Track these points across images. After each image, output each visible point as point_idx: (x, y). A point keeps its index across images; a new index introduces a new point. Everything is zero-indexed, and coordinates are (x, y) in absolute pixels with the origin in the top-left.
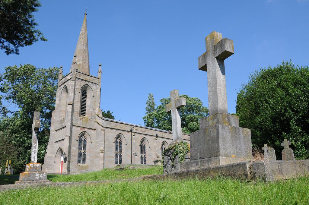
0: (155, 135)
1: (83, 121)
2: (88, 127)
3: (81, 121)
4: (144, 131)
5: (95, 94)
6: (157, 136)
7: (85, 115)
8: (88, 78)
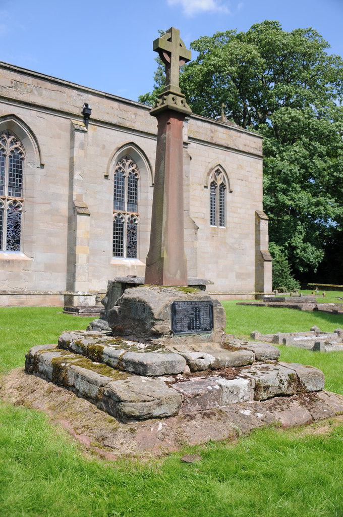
0: (78, 111)
4: (16, 85)
6: (86, 115)
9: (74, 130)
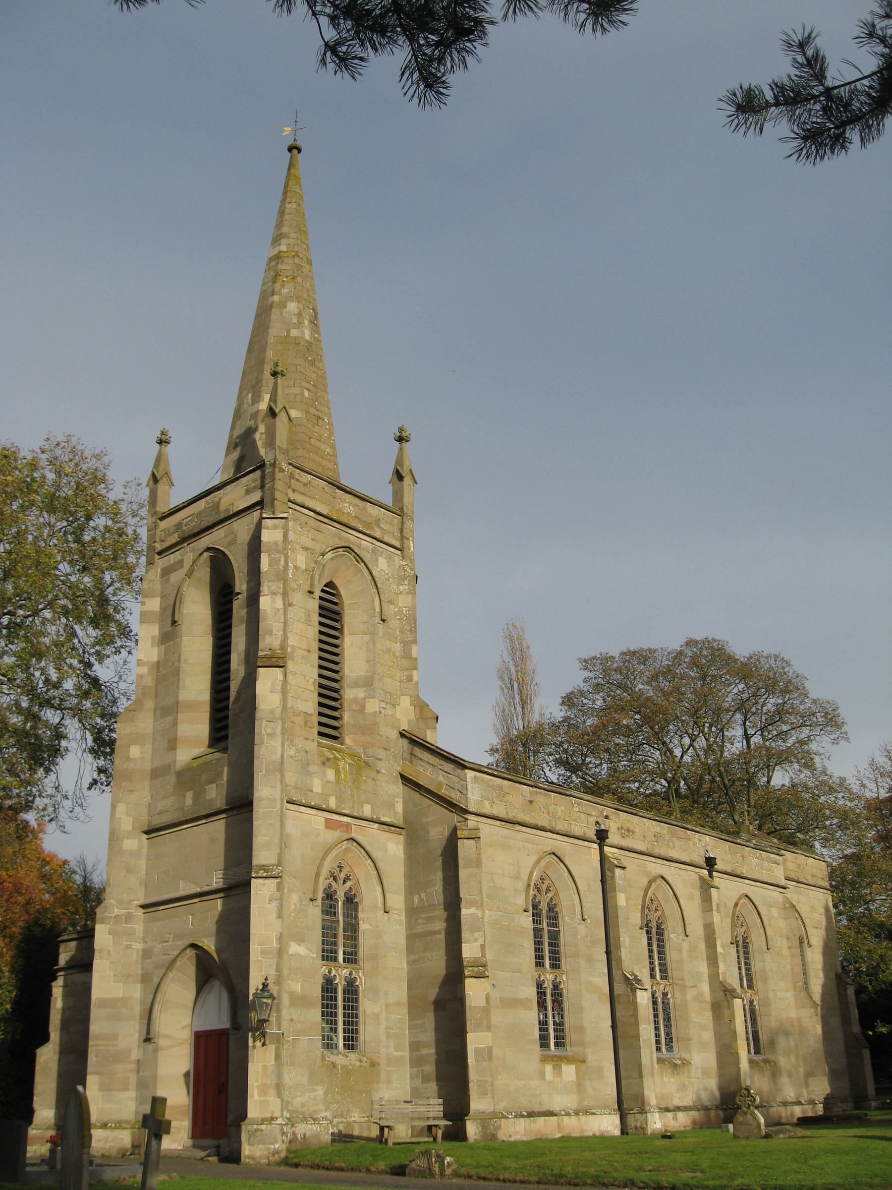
0: (702, 862)
1: (338, 773)
2: (367, 811)
3: (331, 774)
5: (390, 610)
6: (710, 863)
7: (335, 738)
8: (348, 507)
9: (706, 887)
